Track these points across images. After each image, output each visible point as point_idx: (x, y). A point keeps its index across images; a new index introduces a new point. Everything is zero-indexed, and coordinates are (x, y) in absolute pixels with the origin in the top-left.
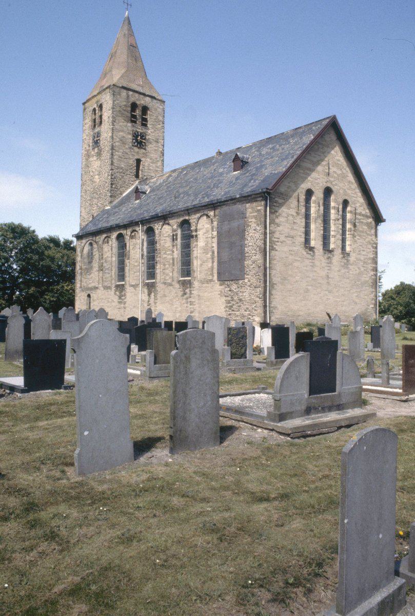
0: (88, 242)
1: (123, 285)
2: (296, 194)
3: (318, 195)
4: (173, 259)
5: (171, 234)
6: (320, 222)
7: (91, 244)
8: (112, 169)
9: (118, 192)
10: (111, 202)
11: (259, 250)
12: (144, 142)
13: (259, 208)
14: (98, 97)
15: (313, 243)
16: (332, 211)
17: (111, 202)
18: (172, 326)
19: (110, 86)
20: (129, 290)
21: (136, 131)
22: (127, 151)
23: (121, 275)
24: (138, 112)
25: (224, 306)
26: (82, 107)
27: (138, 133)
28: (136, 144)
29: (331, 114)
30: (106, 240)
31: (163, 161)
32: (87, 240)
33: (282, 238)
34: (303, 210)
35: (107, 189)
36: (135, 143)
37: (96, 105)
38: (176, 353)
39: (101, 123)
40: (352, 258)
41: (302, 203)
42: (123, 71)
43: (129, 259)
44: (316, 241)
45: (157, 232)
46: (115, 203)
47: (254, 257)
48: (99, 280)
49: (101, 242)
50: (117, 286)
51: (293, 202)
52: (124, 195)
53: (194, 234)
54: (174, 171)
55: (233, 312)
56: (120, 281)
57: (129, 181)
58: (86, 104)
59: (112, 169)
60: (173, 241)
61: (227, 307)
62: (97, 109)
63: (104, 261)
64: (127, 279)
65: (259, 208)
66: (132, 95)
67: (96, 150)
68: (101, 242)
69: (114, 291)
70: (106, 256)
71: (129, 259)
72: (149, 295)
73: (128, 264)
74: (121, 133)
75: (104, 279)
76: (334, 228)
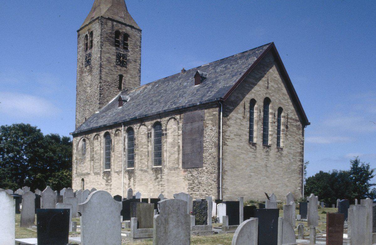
0: (82, 139)
2: (242, 103)
3: (259, 104)
4: (148, 152)
5: (147, 133)
6: (261, 124)
7: (84, 140)
9: (105, 100)
11: (214, 145)
12: (125, 62)
13: (215, 113)
14: (90, 26)
15: (255, 140)
16: (270, 116)
17: (100, 108)
19: (98, 18)
20: (114, 175)
21: (119, 53)
22: (113, 68)
23: (108, 164)
24: (121, 38)
25: (187, 187)
28: (119, 63)
29: (271, 41)
30: (96, 137)
31: (140, 76)
32: (81, 137)
33: (232, 136)
34: (248, 115)
36: (118, 62)
37: (87, 32)
39: (92, 46)
40: (285, 152)
41: (248, 109)
42: (109, 6)
44: (257, 138)
47: (210, 151)
49: (92, 139)
50: (105, 173)
51: (240, 108)
52: (110, 102)
53: (164, 132)
54: (148, 84)
55: (194, 192)
58: (80, 32)
61: (189, 188)
64: (112, 167)
65: (215, 113)
66: (116, 25)
67: (88, 67)
70: (96, 150)
73: (113, 156)
76: (271, 129)
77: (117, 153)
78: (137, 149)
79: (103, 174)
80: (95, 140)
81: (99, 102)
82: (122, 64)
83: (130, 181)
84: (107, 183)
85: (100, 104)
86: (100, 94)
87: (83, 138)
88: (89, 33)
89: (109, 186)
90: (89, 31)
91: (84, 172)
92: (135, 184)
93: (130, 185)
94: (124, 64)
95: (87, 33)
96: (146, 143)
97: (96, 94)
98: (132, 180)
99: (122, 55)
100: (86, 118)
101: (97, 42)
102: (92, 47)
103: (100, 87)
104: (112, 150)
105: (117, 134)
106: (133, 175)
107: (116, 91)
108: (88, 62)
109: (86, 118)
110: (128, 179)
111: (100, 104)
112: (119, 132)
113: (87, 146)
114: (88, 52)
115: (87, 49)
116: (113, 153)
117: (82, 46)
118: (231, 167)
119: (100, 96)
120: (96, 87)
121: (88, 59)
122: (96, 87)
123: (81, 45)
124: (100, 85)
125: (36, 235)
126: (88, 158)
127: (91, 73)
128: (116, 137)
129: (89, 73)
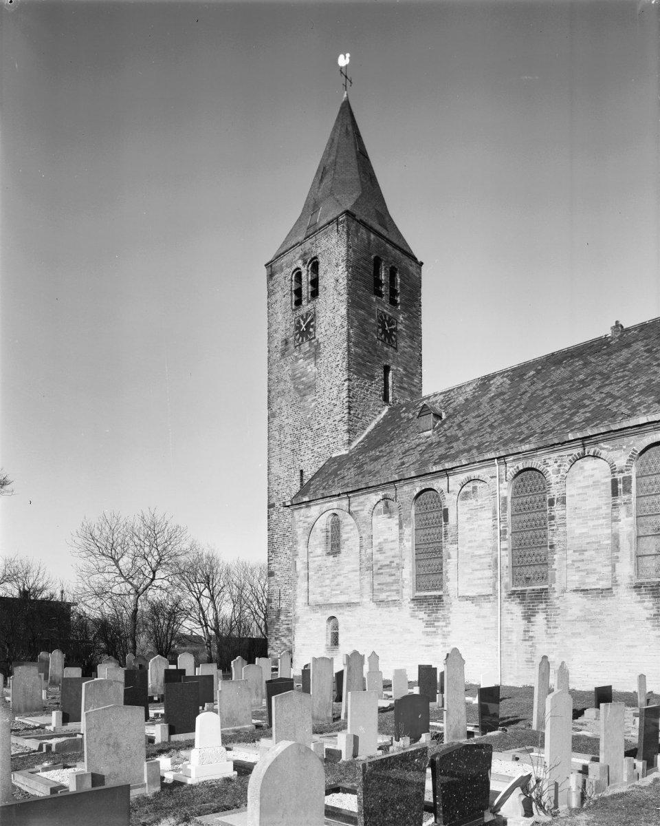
1: (440, 597)
4: (615, 537)
5: (609, 480)
8: (349, 380)
10: (350, 442)
12: (395, 336)
14: (307, 245)
17: (350, 442)
18: (436, 678)
21: (383, 312)
26: (264, 272)
27: (385, 317)
28: (383, 336)
35: (338, 418)
38: (500, 734)
39: (315, 294)
42: (356, 195)
43: (455, 542)
45: (552, 478)
46: (354, 444)
48: (362, 588)
56: (421, 590)
57: (374, 405)
59: (349, 380)
60: (615, 493)
62: (304, 270)
63: (375, 550)
67: (306, 346)
68: (365, 513)
69: (410, 611)
70: (381, 540)
71: (455, 542)
72: (528, 617)
73: (453, 554)
74: (362, 312)
75: (376, 587)
77: (470, 544)
78: (561, 529)
79: (412, 605)
80: (378, 514)
81: (346, 427)
82: (389, 342)
83: (529, 622)
84: (429, 629)
85: (349, 431)
86: (349, 408)
87: (331, 512)
88: (305, 263)
89: (440, 636)
90: (306, 257)
91: (333, 601)
92: (553, 631)
93: (531, 634)
94: (393, 341)
95: (300, 264)
96: (606, 510)
97: (337, 409)
98: (540, 618)
99: (387, 318)
100: (302, 471)
101: (333, 280)
102: (317, 294)
103: (349, 391)
104: (450, 539)
105: (466, 493)
106: (543, 606)
107: (380, 403)
108: (305, 330)
109: (302, 471)
110: (520, 618)
111: (349, 431)
112: (475, 488)
113: (347, 533)
114: (306, 307)
115: (298, 303)
116: (455, 546)
117: (284, 298)
118: (567, 611)
119: (349, 413)
120: (335, 390)
121: (304, 326)
122: (336, 392)
123: (279, 296)
124: (349, 386)
125: (491, 794)
126: (349, 563)
127: (315, 359)
128: (464, 502)
129: (309, 361)
